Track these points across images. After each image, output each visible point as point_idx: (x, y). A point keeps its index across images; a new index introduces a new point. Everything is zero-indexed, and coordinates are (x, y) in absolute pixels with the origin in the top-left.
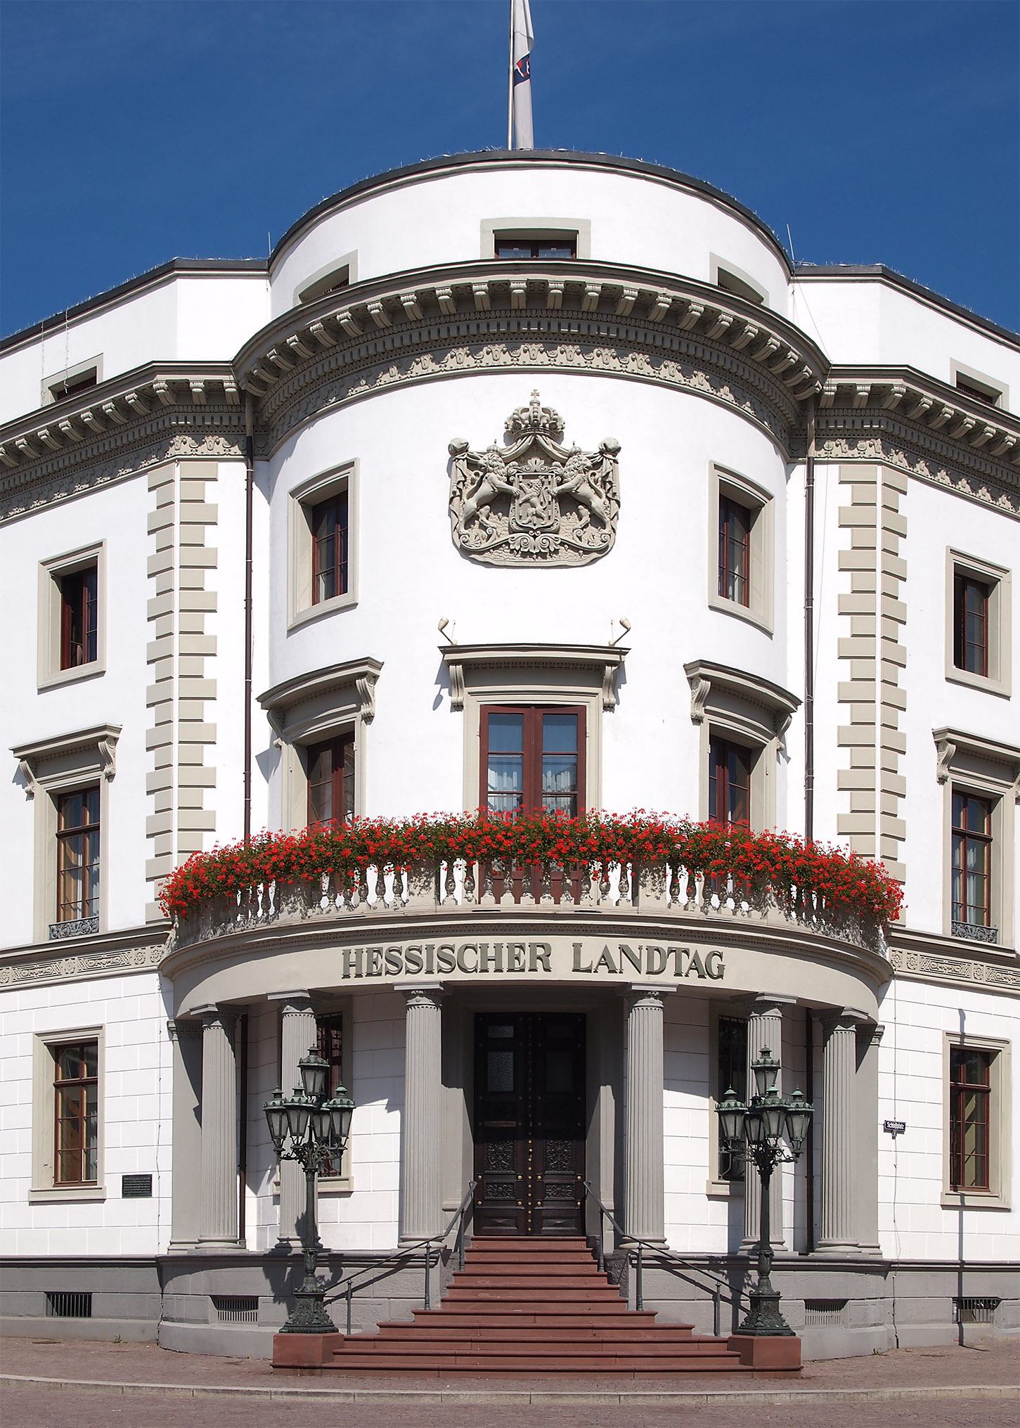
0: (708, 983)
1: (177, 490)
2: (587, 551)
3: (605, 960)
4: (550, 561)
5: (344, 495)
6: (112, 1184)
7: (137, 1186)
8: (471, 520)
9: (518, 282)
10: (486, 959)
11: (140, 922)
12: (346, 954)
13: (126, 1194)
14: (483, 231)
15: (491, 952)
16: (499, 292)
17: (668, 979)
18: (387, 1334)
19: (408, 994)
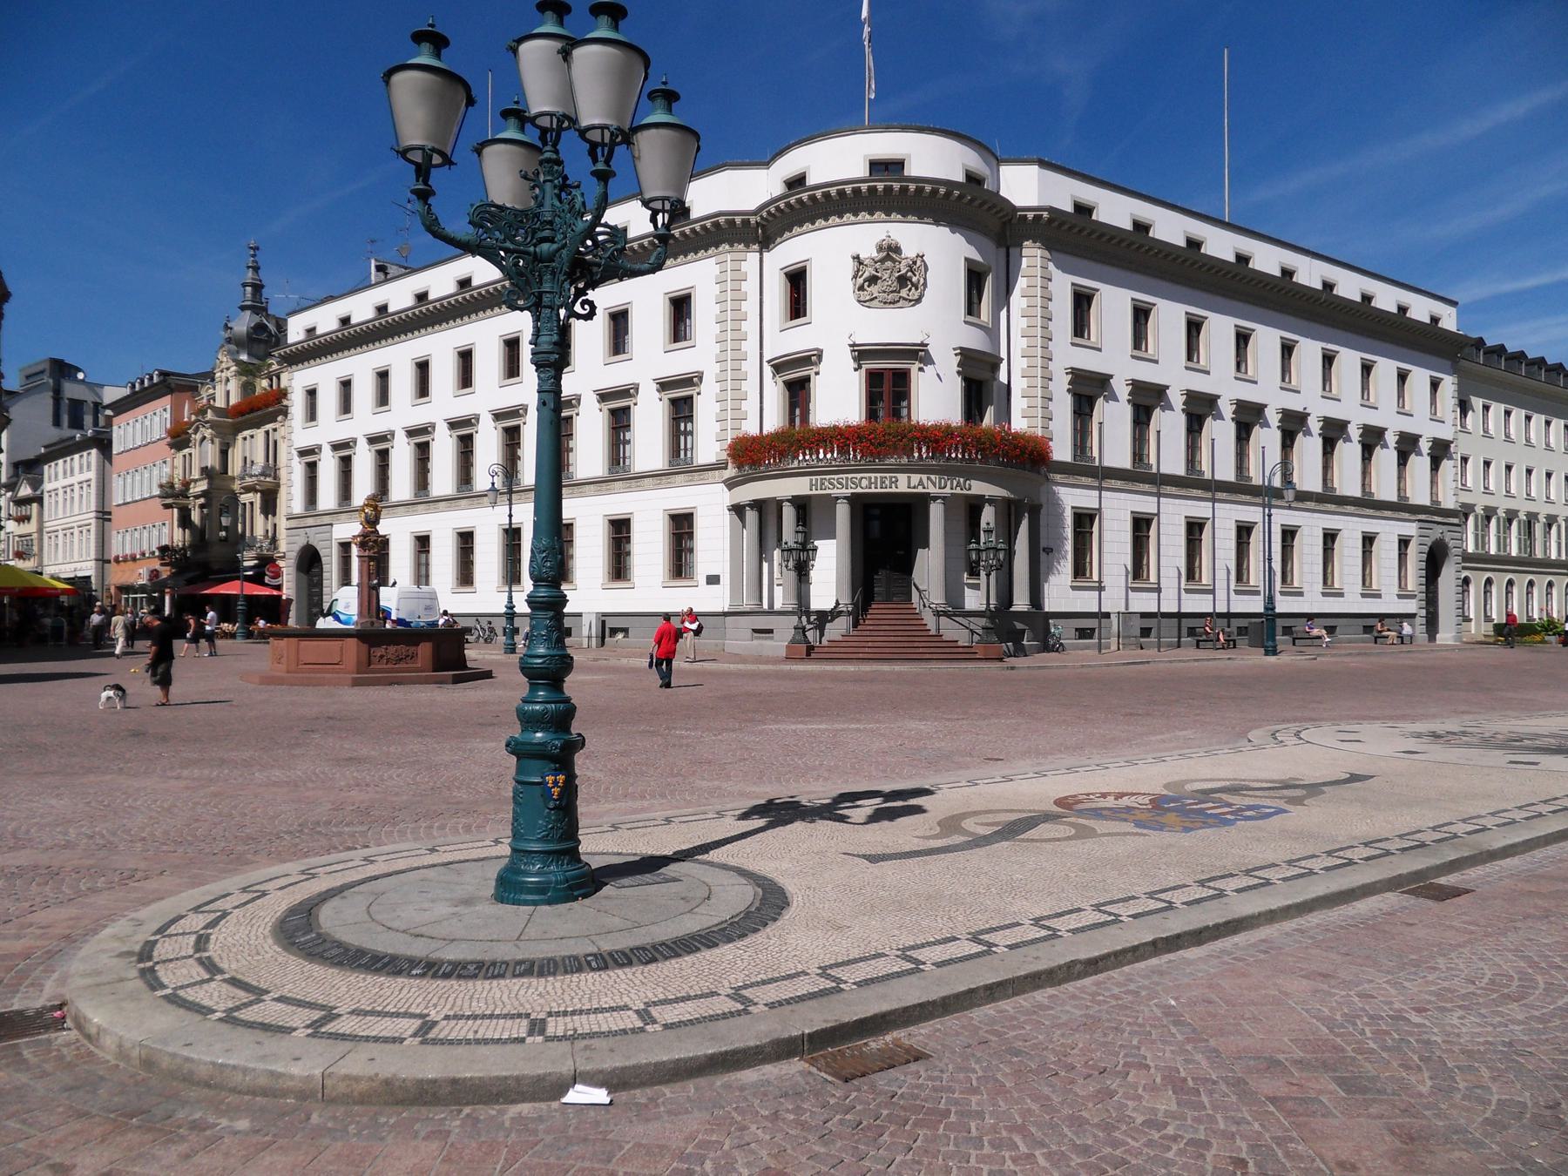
0: (965, 492)
1: (729, 325)
2: (910, 301)
3: (921, 483)
4: (896, 305)
5: (805, 271)
6: (702, 579)
7: (713, 580)
8: (861, 288)
9: (880, 186)
10: (871, 483)
11: (713, 460)
12: (811, 480)
13: (708, 583)
14: (865, 160)
15: (873, 480)
16: (872, 190)
17: (948, 490)
18: (831, 644)
19: (837, 498)
